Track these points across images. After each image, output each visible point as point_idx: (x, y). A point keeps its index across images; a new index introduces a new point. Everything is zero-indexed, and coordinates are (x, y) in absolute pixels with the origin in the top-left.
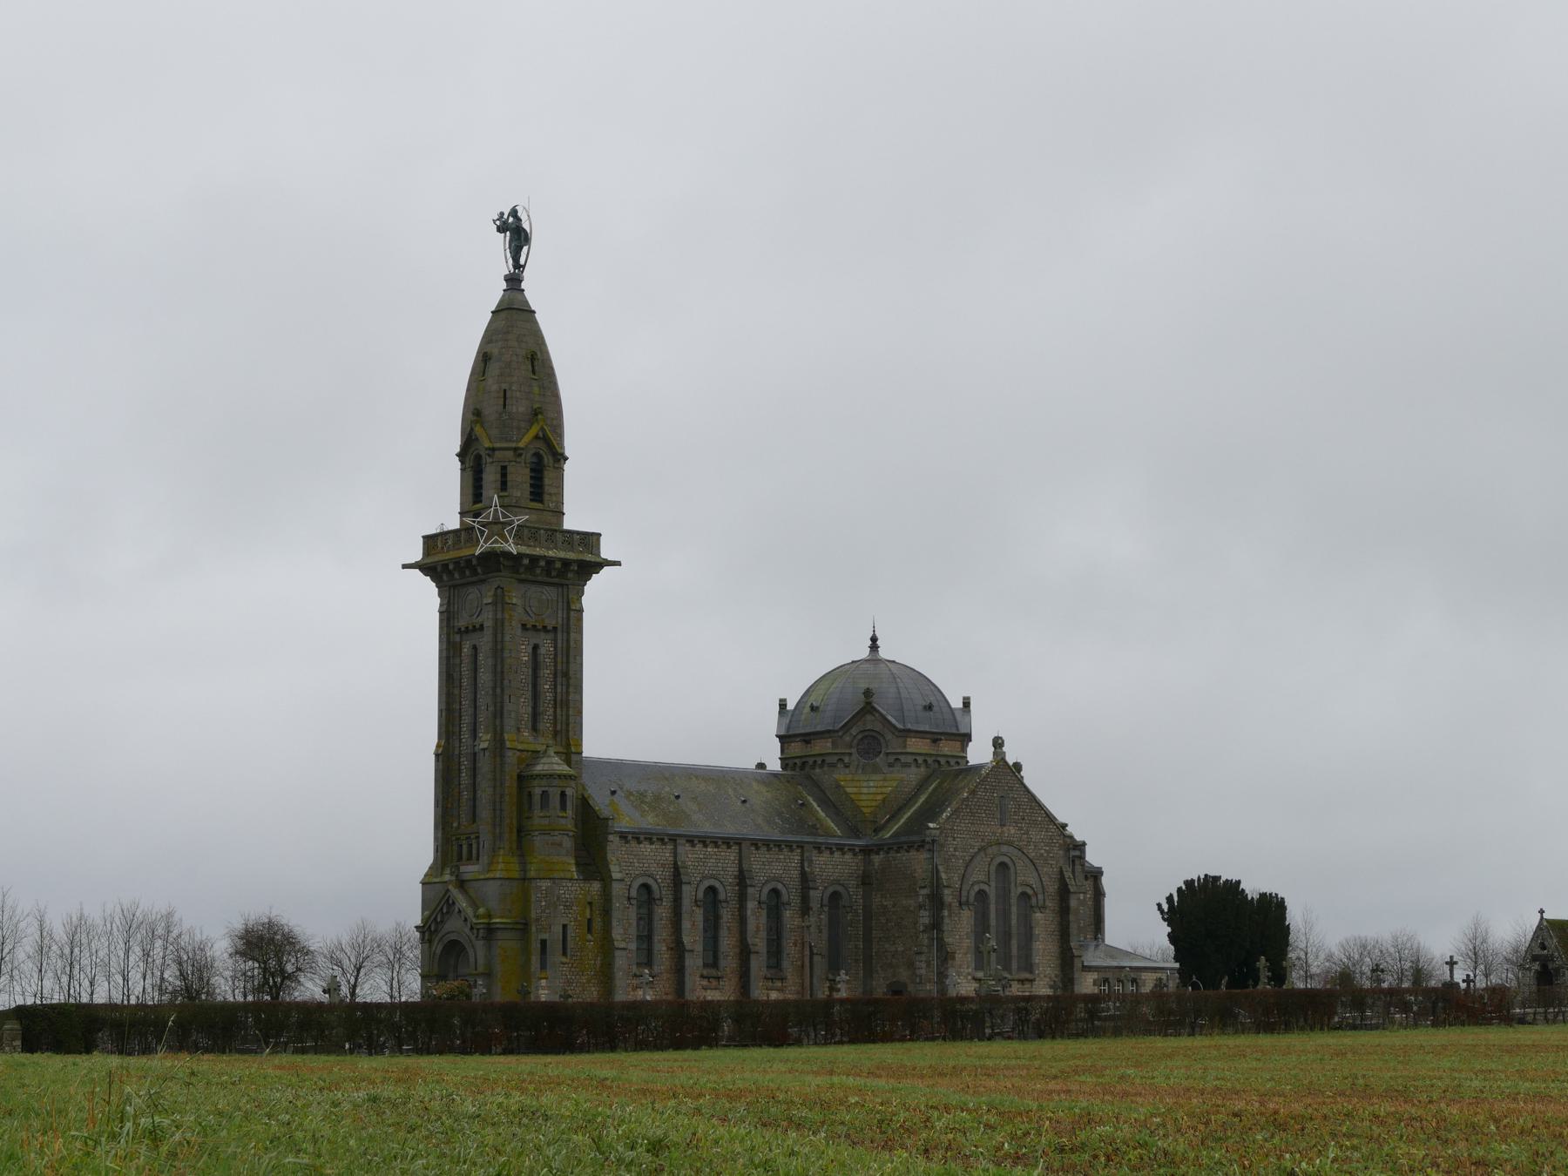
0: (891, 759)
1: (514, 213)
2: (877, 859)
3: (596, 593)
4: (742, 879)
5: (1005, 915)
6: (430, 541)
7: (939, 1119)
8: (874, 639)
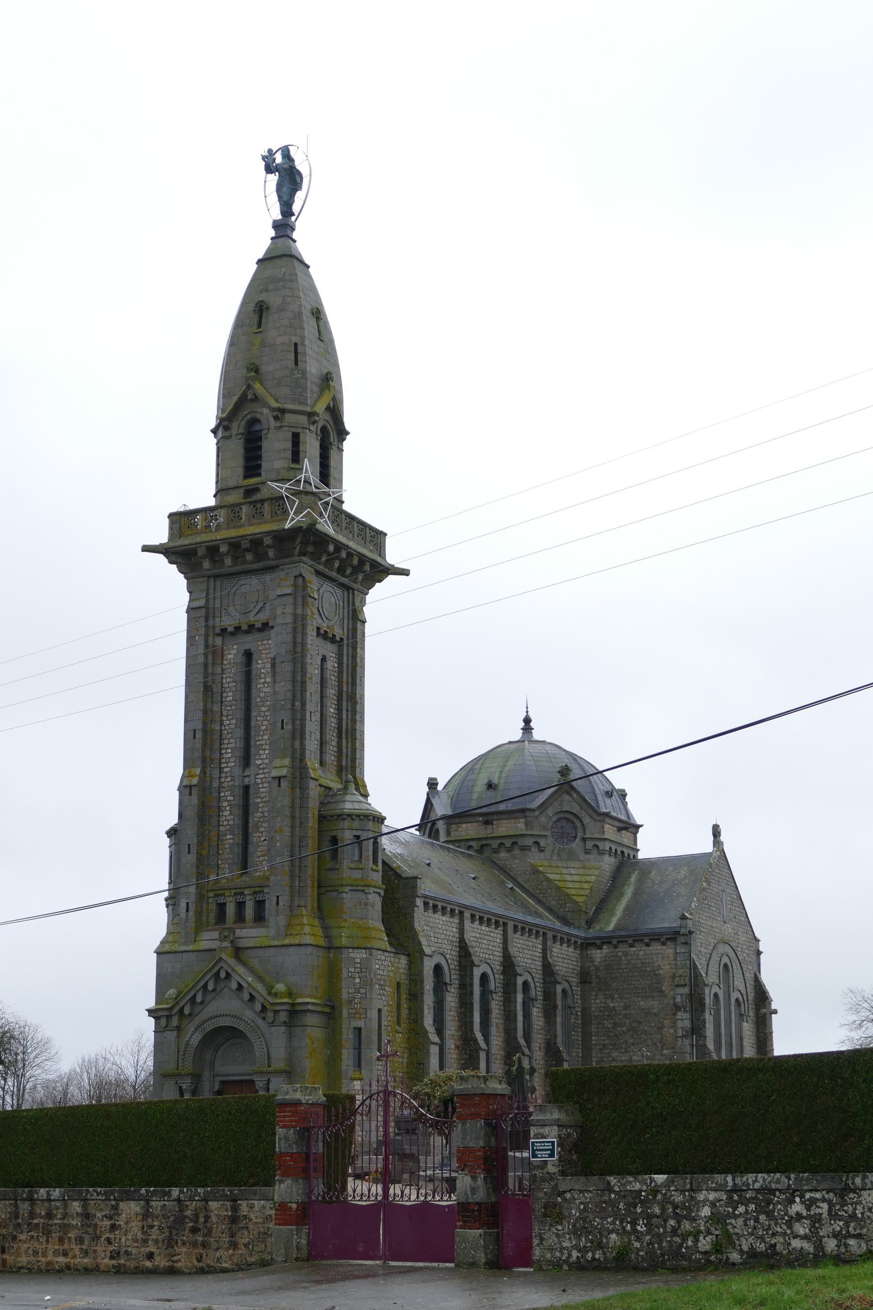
1: (286, 152)
2: (598, 955)
3: (380, 602)
6: (180, 521)
8: (527, 721)
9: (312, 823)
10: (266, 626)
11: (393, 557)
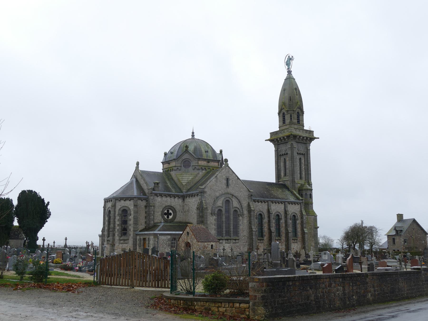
0: (194, 167)
3: (313, 145)
4: (286, 212)
5: (228, 218)
6: (272, 134)
7: (335, 287)
8: (193, 133)
9: (232, 212)
10: (287, 154)
11: (315, 135)
